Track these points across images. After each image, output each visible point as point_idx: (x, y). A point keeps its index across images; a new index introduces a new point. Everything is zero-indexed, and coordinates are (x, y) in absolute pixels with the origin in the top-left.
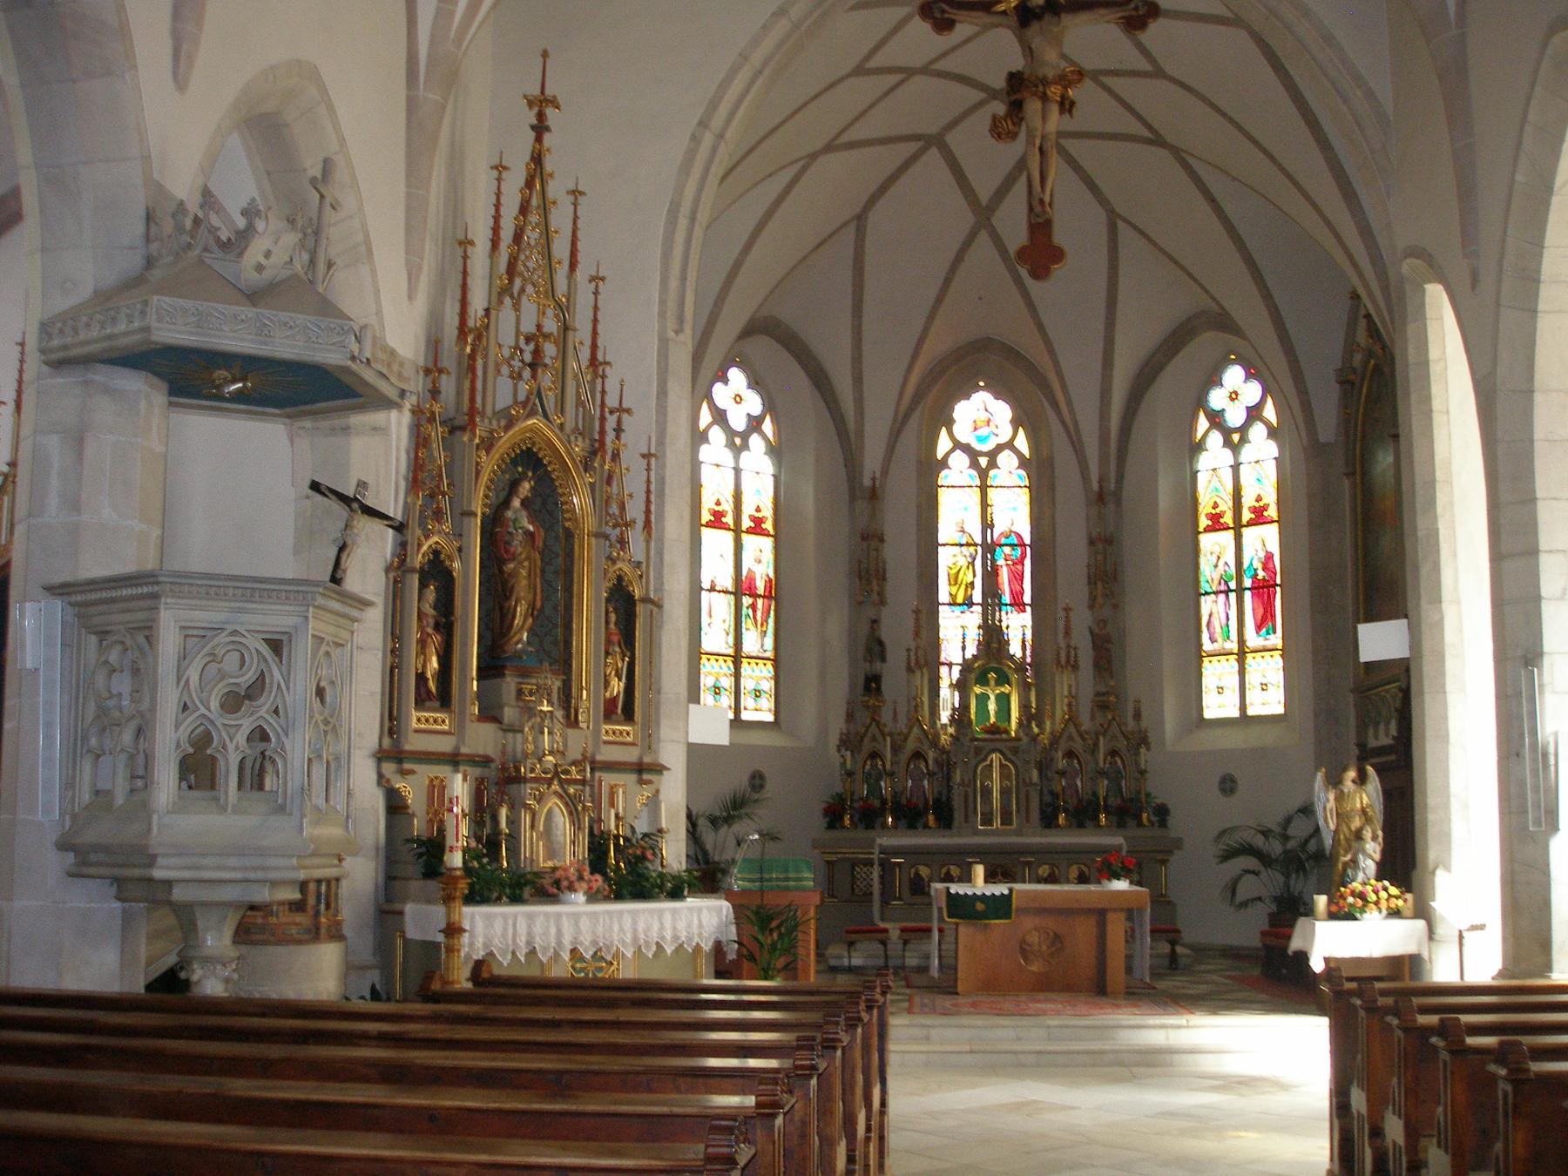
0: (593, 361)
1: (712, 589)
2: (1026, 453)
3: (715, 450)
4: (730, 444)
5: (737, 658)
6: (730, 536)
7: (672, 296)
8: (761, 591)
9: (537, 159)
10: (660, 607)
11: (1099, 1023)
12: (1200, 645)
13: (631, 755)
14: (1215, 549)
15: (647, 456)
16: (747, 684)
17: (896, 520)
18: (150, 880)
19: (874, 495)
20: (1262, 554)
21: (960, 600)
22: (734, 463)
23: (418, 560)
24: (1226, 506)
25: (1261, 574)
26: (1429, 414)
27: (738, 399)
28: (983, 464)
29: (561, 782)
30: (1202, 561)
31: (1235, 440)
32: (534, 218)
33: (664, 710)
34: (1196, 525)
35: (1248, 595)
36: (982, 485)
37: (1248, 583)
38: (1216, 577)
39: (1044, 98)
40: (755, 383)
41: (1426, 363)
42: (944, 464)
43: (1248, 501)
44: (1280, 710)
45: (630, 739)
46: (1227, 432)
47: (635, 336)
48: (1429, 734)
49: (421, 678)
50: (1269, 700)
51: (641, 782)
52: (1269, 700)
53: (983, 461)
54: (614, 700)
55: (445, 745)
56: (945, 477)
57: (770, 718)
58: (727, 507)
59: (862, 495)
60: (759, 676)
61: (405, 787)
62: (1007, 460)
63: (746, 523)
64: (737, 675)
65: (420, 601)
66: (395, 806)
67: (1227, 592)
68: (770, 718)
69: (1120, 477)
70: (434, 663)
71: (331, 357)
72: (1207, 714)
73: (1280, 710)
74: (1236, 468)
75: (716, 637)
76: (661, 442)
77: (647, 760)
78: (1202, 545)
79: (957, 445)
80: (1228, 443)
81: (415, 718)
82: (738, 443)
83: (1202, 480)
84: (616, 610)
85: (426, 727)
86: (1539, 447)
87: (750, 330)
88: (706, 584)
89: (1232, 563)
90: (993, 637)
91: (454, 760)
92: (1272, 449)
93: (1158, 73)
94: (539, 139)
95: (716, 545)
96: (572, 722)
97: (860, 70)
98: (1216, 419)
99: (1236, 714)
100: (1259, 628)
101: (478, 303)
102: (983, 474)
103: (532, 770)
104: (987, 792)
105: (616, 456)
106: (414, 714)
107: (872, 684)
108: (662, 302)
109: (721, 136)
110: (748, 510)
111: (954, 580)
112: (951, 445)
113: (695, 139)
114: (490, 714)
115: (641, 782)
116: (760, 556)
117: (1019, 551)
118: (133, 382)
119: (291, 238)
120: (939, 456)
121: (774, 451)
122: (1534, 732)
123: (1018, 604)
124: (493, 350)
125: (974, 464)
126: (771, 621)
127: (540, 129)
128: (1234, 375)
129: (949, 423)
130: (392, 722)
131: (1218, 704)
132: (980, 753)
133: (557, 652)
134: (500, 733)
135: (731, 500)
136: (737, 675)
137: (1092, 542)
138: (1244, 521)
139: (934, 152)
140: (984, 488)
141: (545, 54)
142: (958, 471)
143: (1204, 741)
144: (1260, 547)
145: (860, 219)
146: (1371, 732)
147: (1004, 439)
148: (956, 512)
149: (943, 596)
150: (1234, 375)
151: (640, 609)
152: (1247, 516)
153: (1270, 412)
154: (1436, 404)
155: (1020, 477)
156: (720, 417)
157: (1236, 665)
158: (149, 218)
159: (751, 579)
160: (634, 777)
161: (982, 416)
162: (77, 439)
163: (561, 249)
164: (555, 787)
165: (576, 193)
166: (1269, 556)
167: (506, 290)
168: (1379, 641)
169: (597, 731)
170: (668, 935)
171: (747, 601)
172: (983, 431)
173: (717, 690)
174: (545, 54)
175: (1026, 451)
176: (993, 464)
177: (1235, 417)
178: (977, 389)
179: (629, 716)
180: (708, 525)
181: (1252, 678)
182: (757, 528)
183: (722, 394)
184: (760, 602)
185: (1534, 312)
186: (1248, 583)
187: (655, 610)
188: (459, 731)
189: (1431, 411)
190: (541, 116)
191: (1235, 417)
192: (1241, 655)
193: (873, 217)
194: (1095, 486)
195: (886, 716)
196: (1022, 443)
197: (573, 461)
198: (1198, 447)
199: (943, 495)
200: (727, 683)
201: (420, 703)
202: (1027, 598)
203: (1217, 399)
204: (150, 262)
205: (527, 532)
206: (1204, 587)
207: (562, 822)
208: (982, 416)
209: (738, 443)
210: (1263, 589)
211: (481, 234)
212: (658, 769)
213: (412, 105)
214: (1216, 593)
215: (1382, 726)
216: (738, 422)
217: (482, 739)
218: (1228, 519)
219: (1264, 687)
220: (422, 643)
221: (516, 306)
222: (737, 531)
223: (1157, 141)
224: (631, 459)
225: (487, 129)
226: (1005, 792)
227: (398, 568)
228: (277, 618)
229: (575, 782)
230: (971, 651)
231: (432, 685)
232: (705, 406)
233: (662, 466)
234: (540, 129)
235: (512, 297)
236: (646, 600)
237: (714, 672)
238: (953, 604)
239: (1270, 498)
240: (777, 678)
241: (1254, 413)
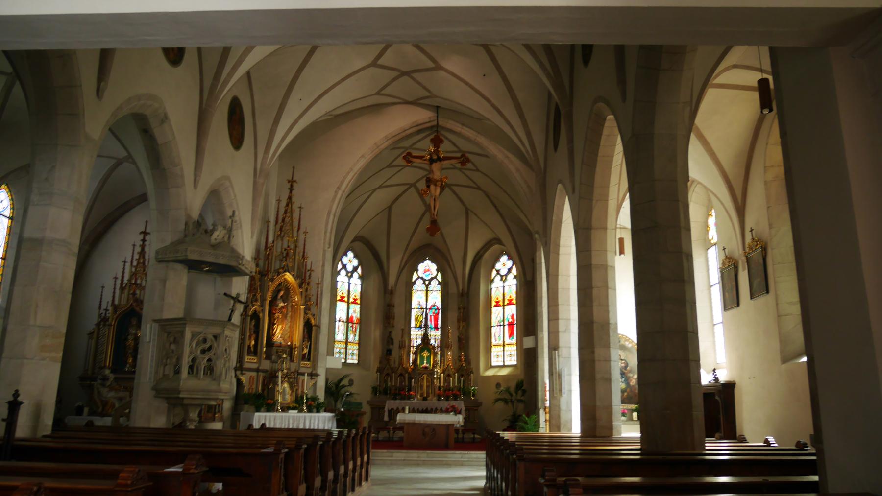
0: (303, 256)
3: (342, 278)
6: (345, 305)
7: (328, 239)
9: (290, 198)
14: (496, 313)
15: (318, 284)
16: (349, 351)
17: (398, 300)
18: (179, 398)
19: (392, 292)
22: (349, 283)
23: (250, 313)
24: (501, 299)
27: (350, 261)
28: (427, 283)
31: (504, 278)
32: (288, 215)
35: (506, 327)
36: (426, 292)
39: (436, 185)
42: (414, 283)
43: (507, 298)
47: (317, 248)
49: (249, 346)
55: (255, 366)
56: (415, 288)
58: (345, 295)
59: (387, 292)
60: (354, 349)
61: (243, 379)
62: (434, 283)
63: (351, 300)
64: (346, 348)
65: (250, 325)
66: (239, 383)
68: (356, 362)
70: (253, 342)
71: (233, 264)
75: (340, 336)
76: (322, 280)
79: (419, 277)
81: (247, 358)
82: (350, 275)
85: (250, 361)
86: (560, 291)
87: (357, 239)
88: (337, 318)
90: (426, 338)
92: (515, 281)
93: (477, 170)
94: (291, 192)
95: (341, 307)
96: (292, 360)
97: (389, 166)
101: (271, 240)
102: (427, 286)
104: (422, 386)
105: (309, 284)
106: (247, 357)
107: (389, 352)
111: (417, 320)
113: (336, 192)
114: (268, 357)
116: (355, 311)
118: (179, 267)
119: (224, 232)
121: (360, 277)
123: (436, 328)
124: (275, 253)
125: (424, 283)
127: (291, 189)
128: (504, 258)
129: (417, 270)
130: (240, 359)
132: (421, 374)
136: (346, 348)
139: (412, 189)
140: (427, 291)
141: (294, 168)
142: (419, 285)
145: (390, 208)
148: (418, 298)
149: (413, 324)
150: (504, 258)
151: (314, 328)
152: (506, 302)
155: (439, 288)
156: (344, 267)
158: (186, 224)
159: (352, 317)
161: (427, 268)
162: (164, 281)
163: (296, 224)
167: (279, 236)
169: (299, 364)
173: (340, 353)
174: (294, 168)
175: (440, 280)
176: (430, 284)
177: (504, 272)
179: (309, 360)
182: (355, 302)
183: (345, 260)
185: (558, 254)
186: (506, 323)
188: (259, 362)
190: (292, 186)
191: (504, 272)
193: (394, 206)
195: (392, 363)
196: (439, 278)
200: (343, 350)
201: (248, 355)
202: (439, 326)
203: (498, 266)
204: (186, 236)
207: (288, 389)
208: (427, 268)
209: (350, 275)
210: (511, 325)
211: (272, 219)
212: (317, 375)
213: (255, 183)
217: (266, 365)
218: (501, 303)
220: (250, 337)
221: (282, 240)
222: (348, 302)
223: (479, 188)
224: (313, 286)
225: (274, 190)
226: (428, 387)
227: (244, 314)
228: (216, 330)
231: (252, 349)
233: (322, 287)
234: (291, 189)
237: (339, 347)
238: (416, 327)
239: (514, 296)
240: (359, 349)
241: (510, 270)
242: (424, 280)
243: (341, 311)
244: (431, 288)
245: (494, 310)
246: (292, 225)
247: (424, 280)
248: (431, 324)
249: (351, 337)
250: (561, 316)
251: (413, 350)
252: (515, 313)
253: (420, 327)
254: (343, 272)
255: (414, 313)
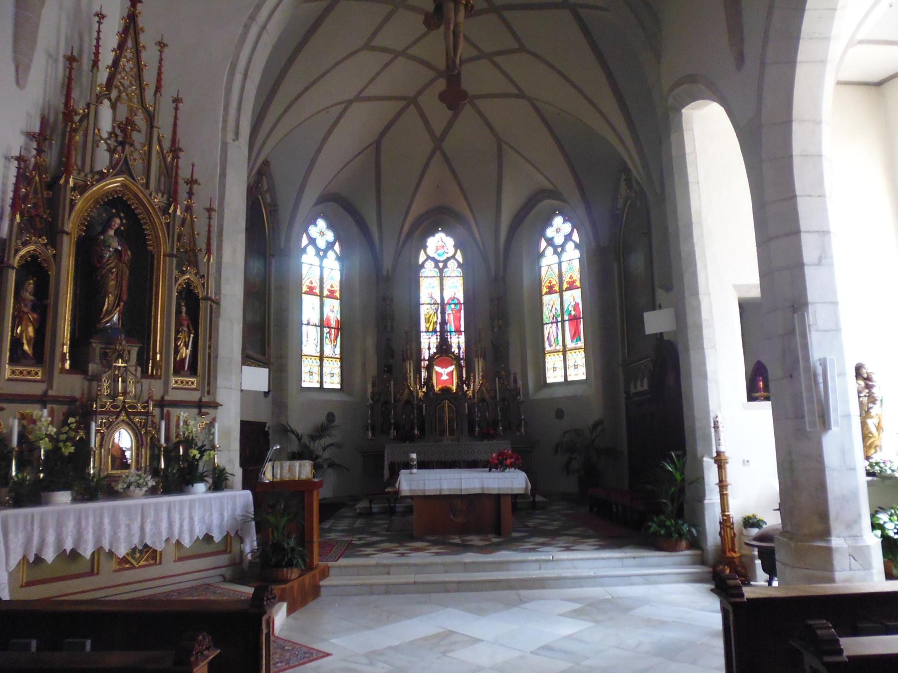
1: (308, 324)
2: (461, 261)
4: (317, 254)
5: (321, 358)
6: (317, 300)
8: (333, 325)
10: (218, 303)
11: (497, 559)
12: (544, 348)
13: (195, 396)
14: (550, 302)
19: (388, 279)
20: (573, 303)
21: (431, 330)
24: (555, 282)
25: (573, 313)
26: (686, 184)
28: (441, 266)
29: (128, 414)
30: (545, 308)
31: (559, 250)
32: (129, 54)
33: (219, 369)
34: (541, 291)
36: (441, 277)
37: (566, 318)
38: (551, 316)
40: (330, 226)
41: (684, 155)
42: (422, 266)
43: (566, 279)
44: (584, 377)
45: (194, 386)
46: (555, 248)
48: (694, 374)
50: (578, 373)
51: (200, 414)
52: (578, 373)
53: (441, 265)
54: (183, 360)
55: (38, 389)
56: (424, 272)
57: (339, 387)
58: (316, 284)
60: (333, 368)
62: (452, 264)
63: (326, 293)
67: (557, 322)
68: (339, 387)
69: (505, 267)
72: (549, 381)
73: (584, 377)
74: (560, 264)
77: (205, 399)
78: (544, 302)
79: (429, 257)
80: (555, 252)
82: (322, 254)
83: (544, 271)
84: (186, 305)
86: (797, 161)
88: (305, 322)
89: (559, 308)
91: (43, 400)
92: (577, 254)
98: (550, 242)
99: (562, 380)
100: (573, 338)
102: (441, 271)
103: (103, 406)
104: (442, 420)
108: (225, 121)
109: (264, 28)
110: (327, 287)
111: (428, 320)
112: (425, 257)
115: (200, 414)
116: (333, 310)
117: (458, 307)
120: (420, 262)
121: (339, 258)
122: (807, 358)
123: (458, 331)
125: (437, 266)
126: (339, 340)
128: (558, 221)
131: (554, 376)
133: (138, 325)
134: (86, 383)
135: (318, 282)
137: (492, 301)
138: (564, 288)
142: (429, 270)
143: (544, 394)
144: (572, 300)
145: (377, 144)
146: (632, 386)
147: (450, 255)
149: (423, 328)
152: (565, 286)
153: (576, 237)
154: (691, 178)
156: (312, 241)
157: (562, 357)
159: (328, 320)
160: (196, 411)
163: (149, 76)
164: (123, 417)
165: (162, 45)
166: (577, 304)
168: (655, 322)
170: (216, 521)
171: (326, 330)
172: (441, 251)
173: (311, 373)
175: (461, 261)
176: (445, 266)
178: (438, 231)
179: (193, 371)
180: (306, 293)
181: (570, 363)
182: (331, 296)
183: (313, 231)
184: (333, 331)
186: (566, 318)
187: (214, 306)
189: (688, 182)
191: (559, 240)
192: (564, 352)
194: (493, 274)
197: (154, 209)
198: (542, 255)
199: (421, 279)
200: (316, 369)
203: (550, 232)
205: (116, 250)
206: (546, 320)
209: (322, 254)
210: (574, 319)
212: (215, 405)
214: (552, 323)
215: (639, 382)
216: (321, 244)
218: (557, 288)
219: (576, 367)
222: (321, 296)
223: (521, 95)
229: (140, 414)
230: (433, 350)
232: (305, 235)
235: (110, 99)
236: (207, 298)
238: (427, 331)
239: (577, 276)
240: (342, 367)
241: (568, 237)
242: (437, 262)
243: (310, 309)
244: (447, 272)
245: (546, 299)
246: (139, 77)
247: (437, 262)
248: (451, 327)
249: (328, 350)
250: (805, 224)
251: (425, 364)
252: (579, 301)
253: (434, 331)
254: (311, 250)
255: (424, 311)
